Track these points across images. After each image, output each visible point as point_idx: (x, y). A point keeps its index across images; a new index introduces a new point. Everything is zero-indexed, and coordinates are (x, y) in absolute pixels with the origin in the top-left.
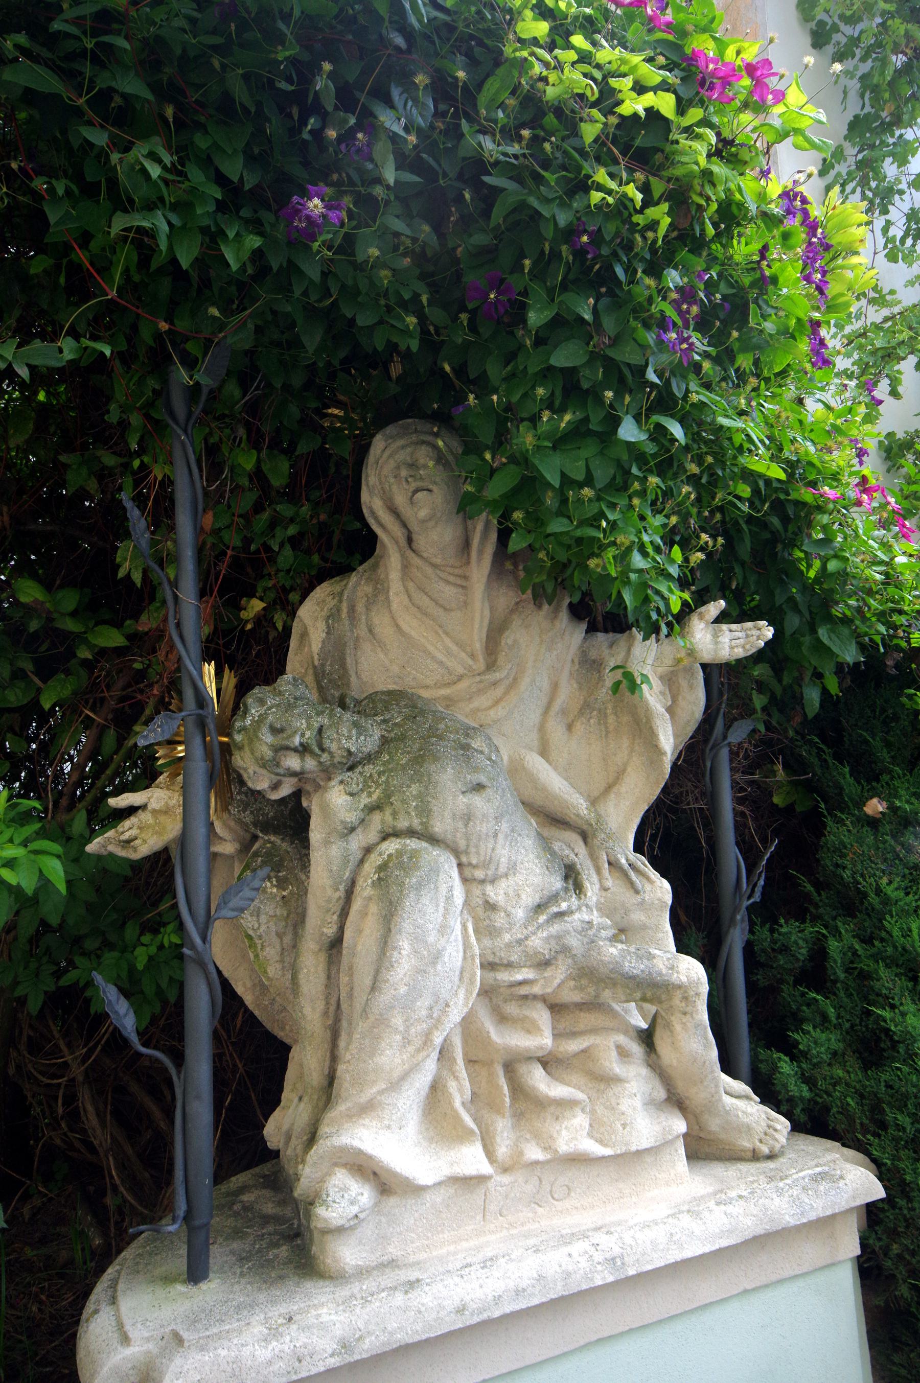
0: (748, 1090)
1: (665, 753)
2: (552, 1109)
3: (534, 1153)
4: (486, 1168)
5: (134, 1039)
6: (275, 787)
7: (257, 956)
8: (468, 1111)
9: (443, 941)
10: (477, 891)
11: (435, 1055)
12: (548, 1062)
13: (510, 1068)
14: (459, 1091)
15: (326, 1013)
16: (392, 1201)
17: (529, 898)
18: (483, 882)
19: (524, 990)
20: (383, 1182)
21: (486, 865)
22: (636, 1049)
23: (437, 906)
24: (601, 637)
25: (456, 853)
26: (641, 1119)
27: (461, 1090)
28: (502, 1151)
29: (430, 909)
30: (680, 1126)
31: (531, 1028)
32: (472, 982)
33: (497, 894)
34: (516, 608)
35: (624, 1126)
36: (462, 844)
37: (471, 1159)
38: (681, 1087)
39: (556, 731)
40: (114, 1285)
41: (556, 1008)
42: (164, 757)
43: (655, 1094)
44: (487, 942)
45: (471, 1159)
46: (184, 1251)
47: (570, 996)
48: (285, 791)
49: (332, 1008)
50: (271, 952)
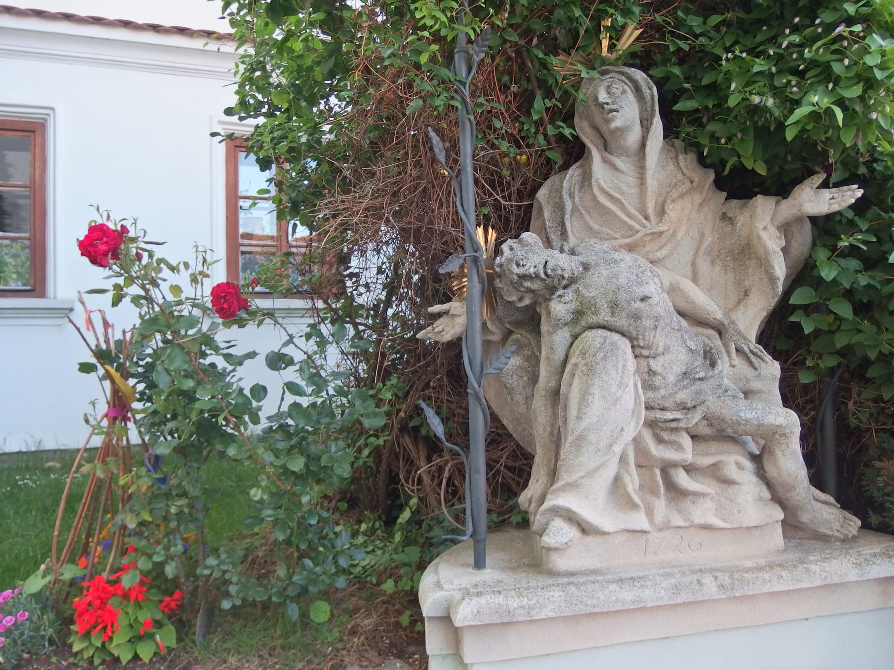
0: (832, 500)
1: (778, 279)
2: (691, 497)
3: (678, 521)
4: (646, 526)
5: (443, 438)
6: (521, 299)
7: (512, 400)
8: (637, 494)
9: (620, 392)
10: (644, 363)
11: (616, 460)
12: (689, 469)
13: (664, 471)
14: (632, 482)
15: (552, 434)
16: (589, 539)
17: (679, 369)
18: (648, 357)
19: (673, 425)
20: (585, 529)
21: (648, 347)
22: (748, 464)
23: (617, 370)
24: (735, 203)
25: (631, 339)
26: (749, 501)
27: (632, 481)
28: (659, 518)
29: (612, 372)
30: (781, 515)
31: (680, 448)
32: (639, 417)
33: (656, 365)
34: (777, 203)
35: (739, 511)
36: (634, 333)
37: (639, 520)
38: (781, 492)
39: (704, 266)
40: (437, 565)
41: (693, 437)
42: (456, 285)
43: (762, 494)
44: (650, 394)
45: (639, 520)
46: (471, 552)
47: (704, 430)
48: (527, 302)
49: (556, 432)
50: (520, 398)
